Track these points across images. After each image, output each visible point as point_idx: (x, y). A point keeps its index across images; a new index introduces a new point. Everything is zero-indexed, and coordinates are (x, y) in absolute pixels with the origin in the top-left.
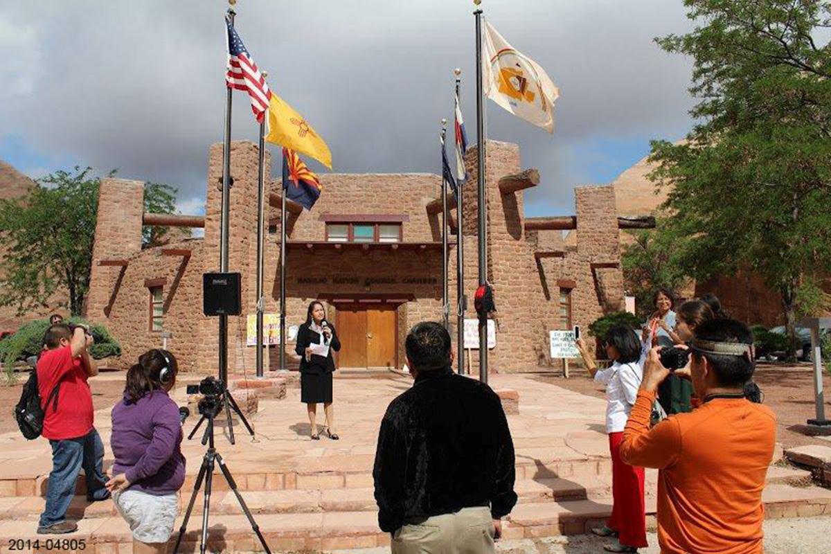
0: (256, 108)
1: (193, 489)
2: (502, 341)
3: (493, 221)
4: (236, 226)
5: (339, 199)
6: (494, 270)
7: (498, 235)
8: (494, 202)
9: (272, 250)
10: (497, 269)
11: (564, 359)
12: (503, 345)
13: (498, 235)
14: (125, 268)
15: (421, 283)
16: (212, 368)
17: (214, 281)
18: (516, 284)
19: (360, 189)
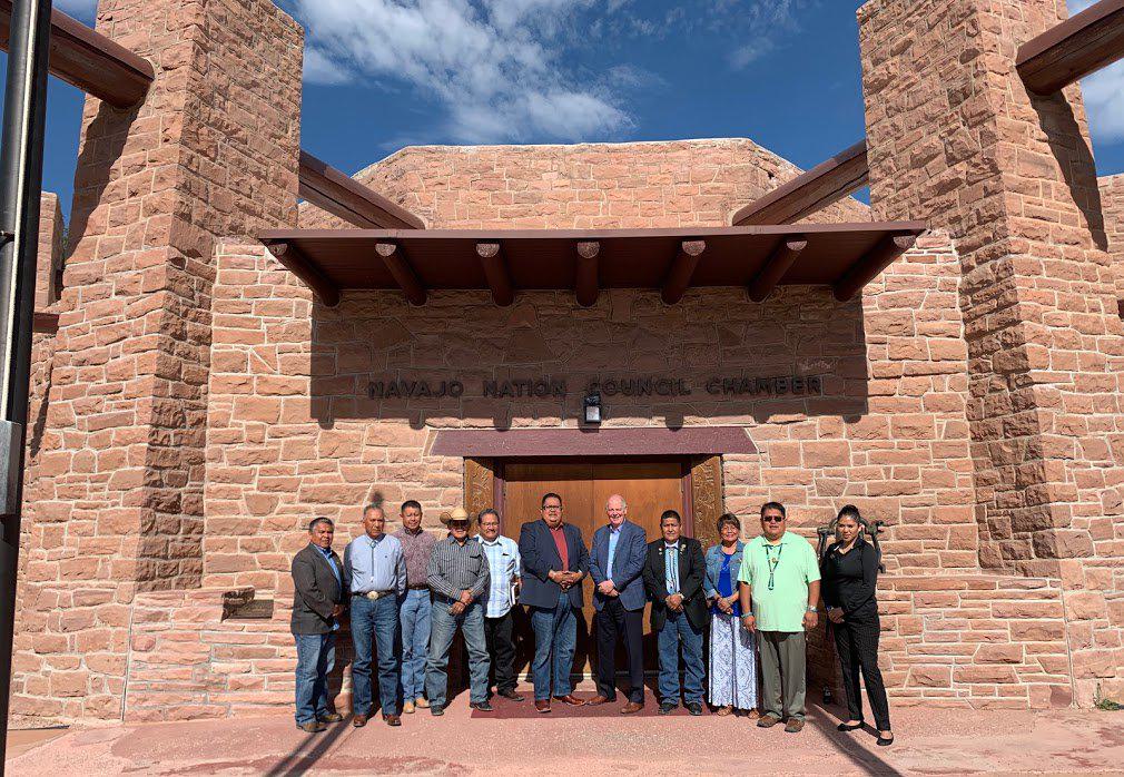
0: (405, 228)
1: (708, 462)
2: (1078, 586)
3: (1011, 175)
4: (156, 211)
5: (512, 208)
6: (1027, 337)
7: (1029, 222)
8: (1009, 119)
9: (285, 294)
10: (1037, 336)
11: (198, 555)
12: (1087, 599)
13: (1029, 222)
14: (580, 586)
15: (769, 392)
16: (55, 693)
17: (551, 572)
18: (1099, 389)
19: (567, 182)
